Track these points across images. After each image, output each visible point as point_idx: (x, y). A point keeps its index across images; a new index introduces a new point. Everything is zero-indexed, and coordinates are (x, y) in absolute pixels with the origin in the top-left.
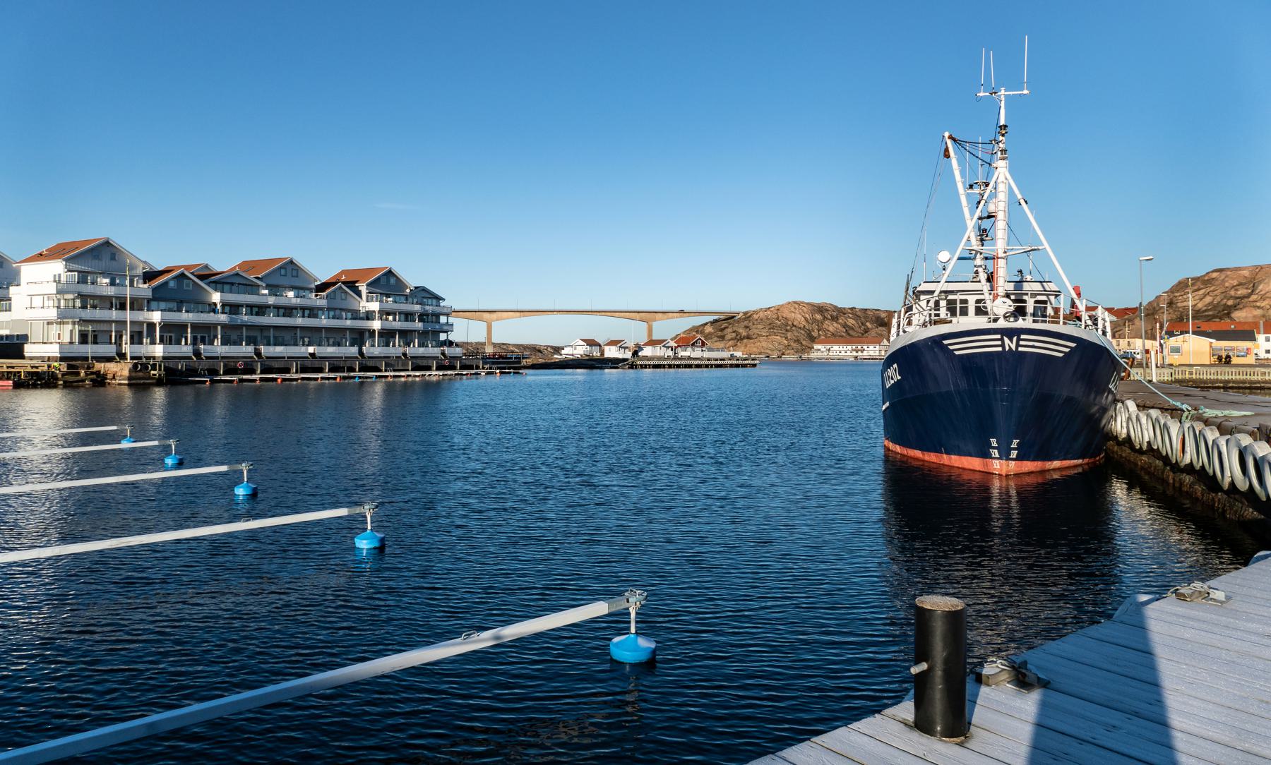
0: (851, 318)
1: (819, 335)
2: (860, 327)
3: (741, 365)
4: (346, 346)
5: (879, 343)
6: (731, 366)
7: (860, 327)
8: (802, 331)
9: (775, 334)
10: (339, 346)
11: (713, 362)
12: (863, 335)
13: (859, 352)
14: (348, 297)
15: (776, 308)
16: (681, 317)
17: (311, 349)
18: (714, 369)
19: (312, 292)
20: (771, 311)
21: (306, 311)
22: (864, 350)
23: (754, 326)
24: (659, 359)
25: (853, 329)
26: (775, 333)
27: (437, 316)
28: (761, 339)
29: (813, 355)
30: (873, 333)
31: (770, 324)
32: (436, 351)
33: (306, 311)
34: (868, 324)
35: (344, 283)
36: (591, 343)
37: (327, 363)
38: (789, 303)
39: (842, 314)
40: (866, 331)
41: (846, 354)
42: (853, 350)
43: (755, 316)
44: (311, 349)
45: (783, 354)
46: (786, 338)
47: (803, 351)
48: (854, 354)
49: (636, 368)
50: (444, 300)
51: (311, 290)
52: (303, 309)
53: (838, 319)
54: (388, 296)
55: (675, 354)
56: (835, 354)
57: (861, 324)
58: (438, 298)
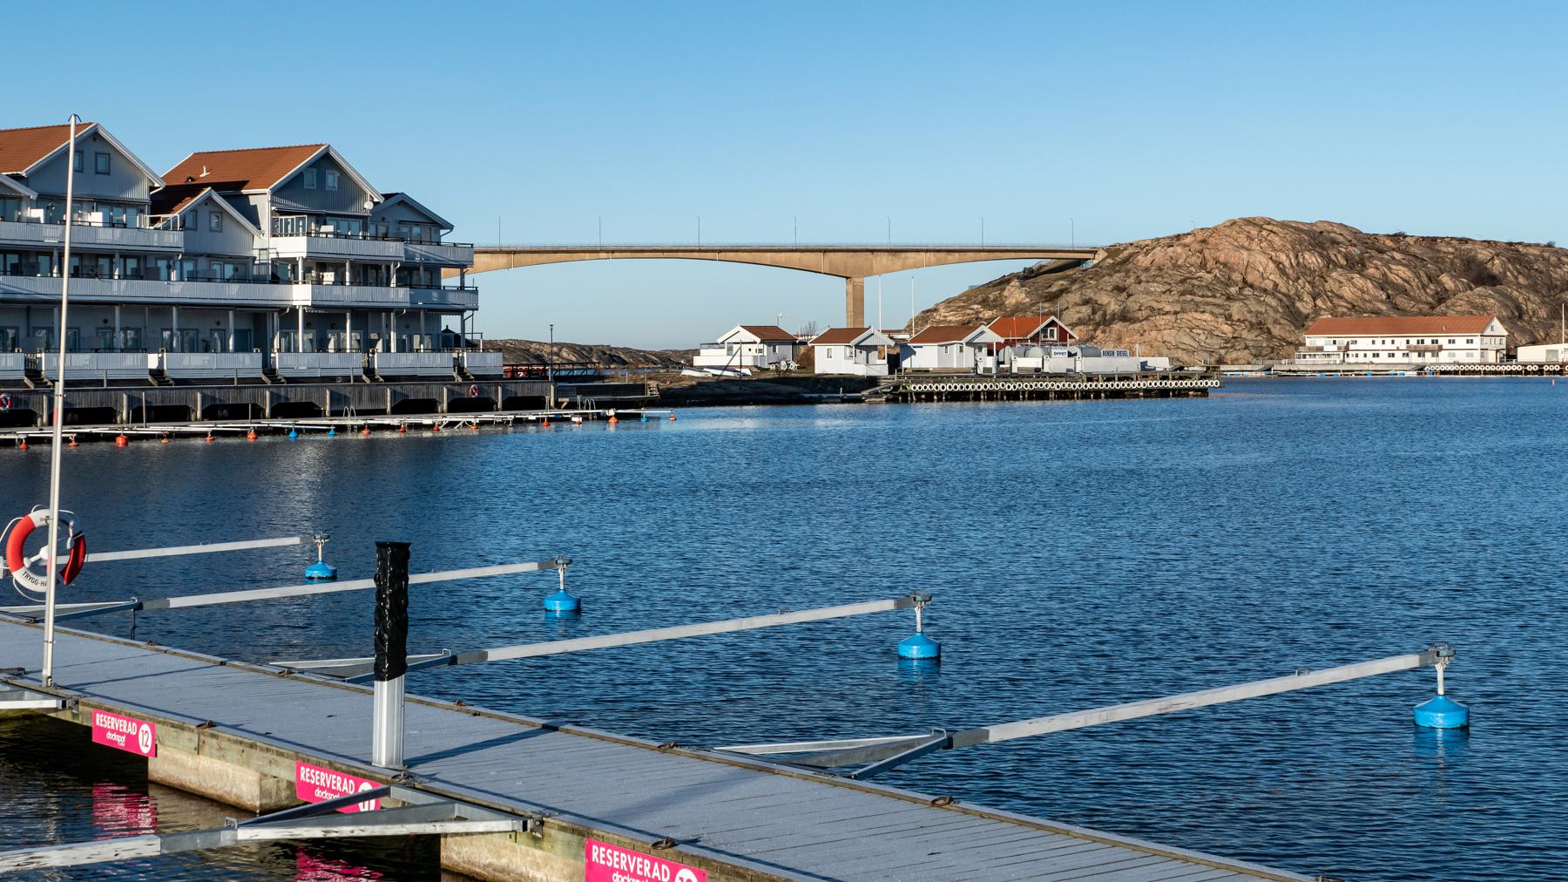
0: (1399, 263)
1: (1316, 310)
2: (1424, 287)
3: (1174, 390)
4: (225, 349)
5: (1481, 331)
6: (1148, 393)
7: (1424, 287)
8: (1269, 299)
9: (1197, 307)
10: (207, 350)
11: (1101, 385)
12: (1433, 308)
13: (1428, 355)
14: (227, 223)
15: (1200, 238)
16: (939, 263)
17: (153, 361)
18: (1102, 402)
19: (142, 211)
20: (1185, 245)
21: (128, 261)
22: (1441, 349)
23: (1141, 288)
24: (963, 376)
25: (1405, 292)
26: (1197, 304)
27: (434, 269)
28: (1161, 320)
29: (1302, 364)
30: (1460, 303)
31: (1183, 282)
32: (441, 362)
33: (8, 256)
34: (1446, 279)
35: (217, 187)
36: (770, 336)
37: (199, 396)
38: (1234, 223)
39: (1374, 253)
40: (1442, 297)
41: (1392, 360)
42: (1411, 349)
43: (1143, 261)
44: (153, 361)
45: (1221, 361)
46: (1229, 318)
47: (1274, 353)
48: (1414, 358)
49: (905, 400)
50: (451, 227)
51: (138, 206)
52: (126, 255)
53: (1364, 265)
54: (321, 219)
55: (999, 363)
56: (1361, 359)
57: (1425, 280)
58: (436, 224)
